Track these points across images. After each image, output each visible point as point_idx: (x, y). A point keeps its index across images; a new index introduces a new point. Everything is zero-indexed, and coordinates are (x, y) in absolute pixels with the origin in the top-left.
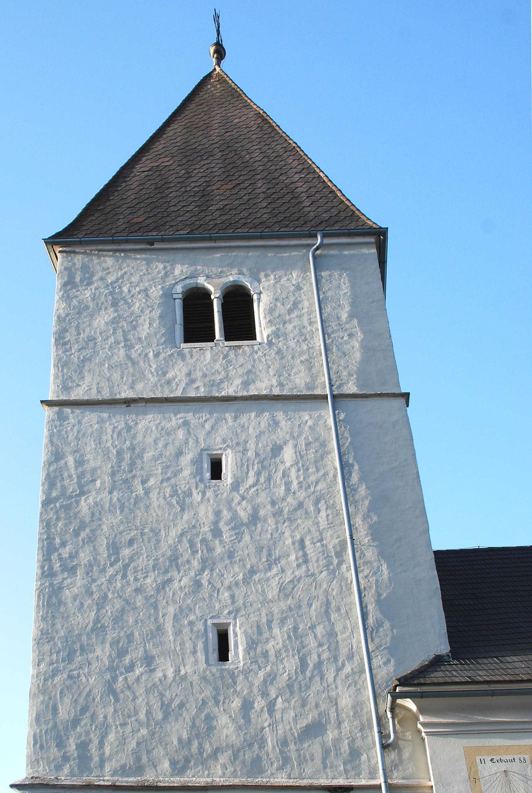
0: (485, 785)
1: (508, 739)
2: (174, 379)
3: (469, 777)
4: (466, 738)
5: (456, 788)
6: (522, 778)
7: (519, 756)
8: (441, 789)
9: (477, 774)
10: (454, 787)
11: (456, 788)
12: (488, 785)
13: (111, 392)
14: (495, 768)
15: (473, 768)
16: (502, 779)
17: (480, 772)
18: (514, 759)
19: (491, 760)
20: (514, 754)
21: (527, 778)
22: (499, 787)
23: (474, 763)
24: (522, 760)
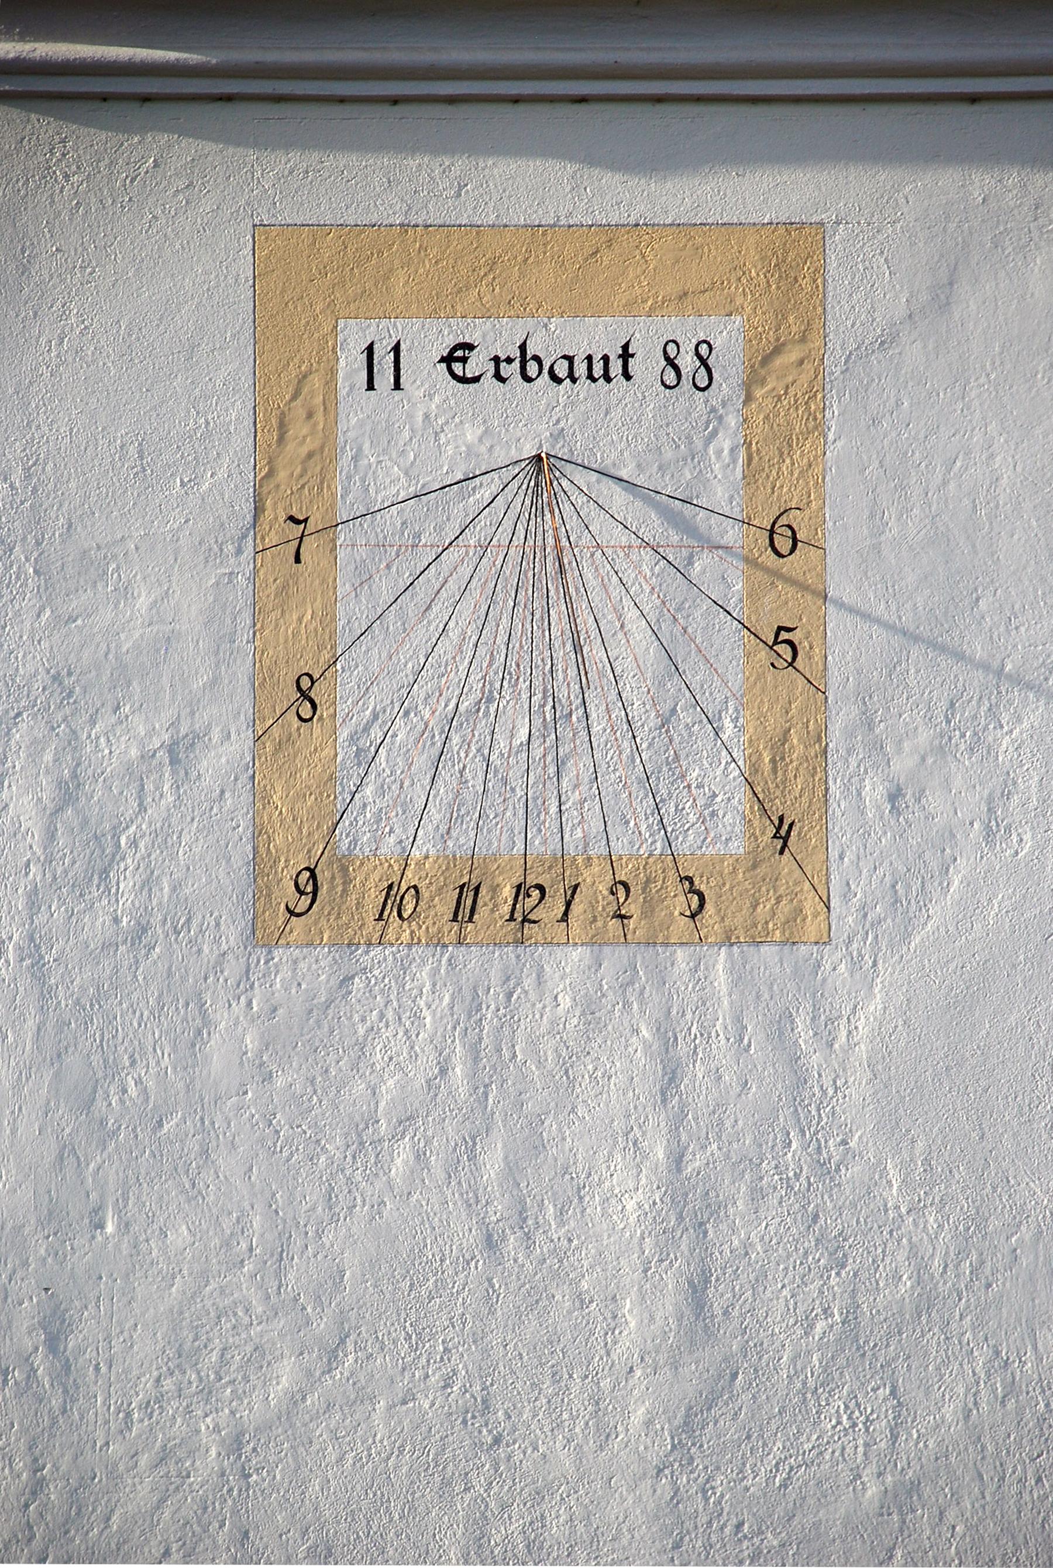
0: (364, 580)
1: (614, 166)
2: (910, 332)
3: (258, 510)
4: (288, 145)
5: (143, 602)
6: (654, 527)
7: (670, 326)
8: (29, 603)
9: (324, 480)
10: (125, 592)
11: (143, 602)
12: (385, 588)
13: (759, 950)
14: (471, 434)
15: (298, 429)
16: (503, 535)
17: (345, 461)
18: (626, 355)
19: (448, 360)
20: (630, 308)
21: (689, 529)
22: (466, 608)
23: (316, 382)
24: (687, 362)
